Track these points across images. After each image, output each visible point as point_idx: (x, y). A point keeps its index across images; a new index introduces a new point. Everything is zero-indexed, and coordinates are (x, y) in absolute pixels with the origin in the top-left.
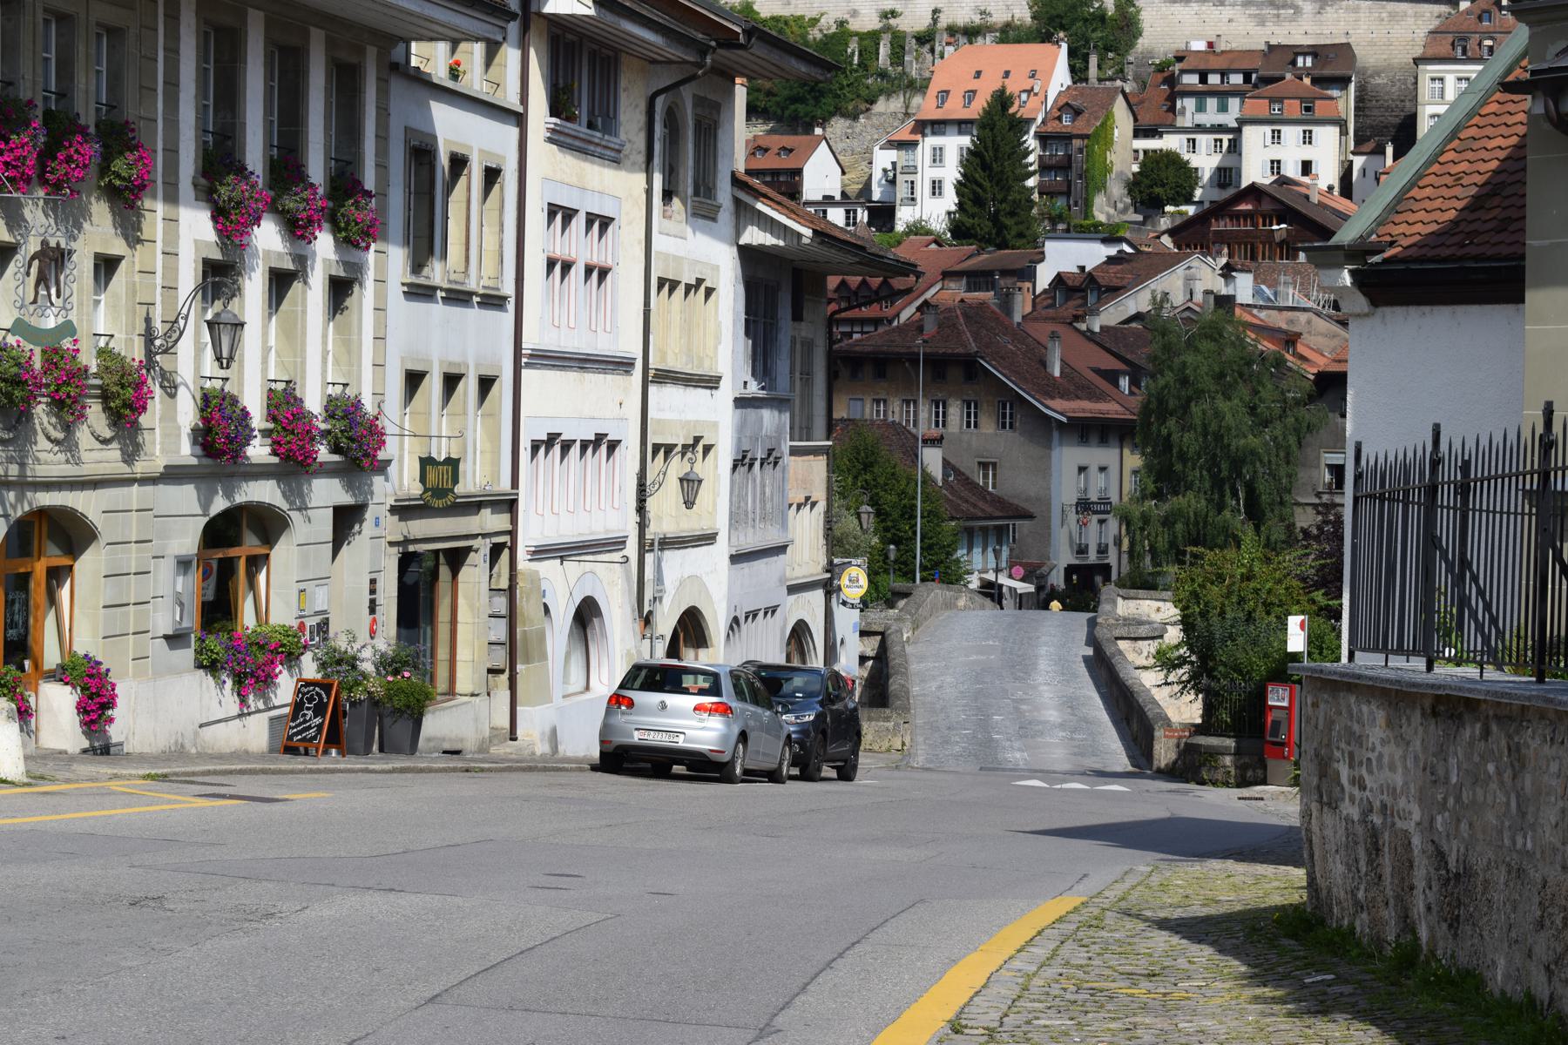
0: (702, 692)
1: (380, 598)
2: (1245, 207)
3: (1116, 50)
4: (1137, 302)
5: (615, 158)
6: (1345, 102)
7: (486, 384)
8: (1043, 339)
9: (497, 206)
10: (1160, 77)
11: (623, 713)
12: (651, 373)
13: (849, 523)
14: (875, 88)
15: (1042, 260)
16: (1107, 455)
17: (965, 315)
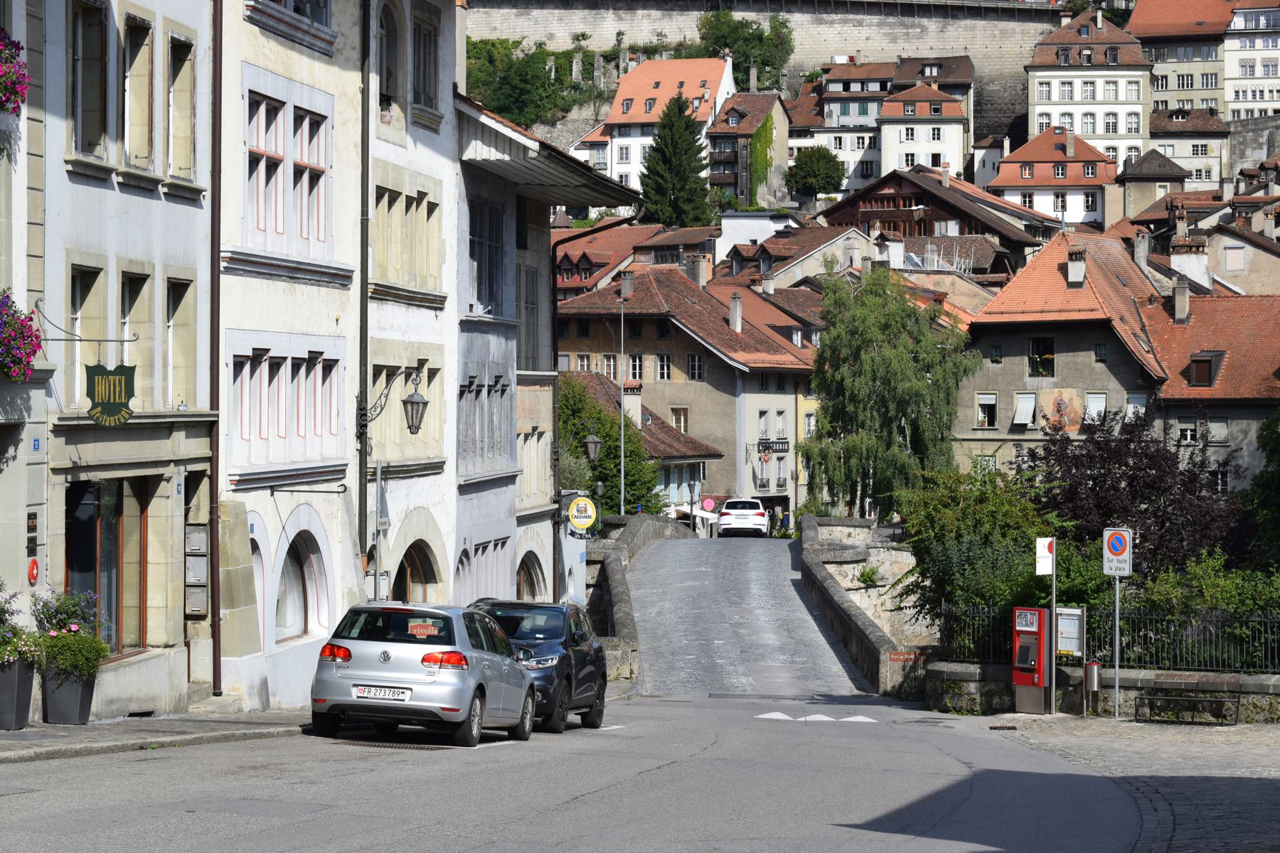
0: (430, 640)
1: (42, 536)
2: (888, 191)
3: (772, 65)
4: (810, 266)
5: (327, 51)
6: (966, 105)
7: (177, 289)
8: (725, 300)
9: (188, 87)
10: (810, 86)
11: (339, 667)
12: (371, 288)
13: (567, 460)
14: (569, 99)
15: (719, 236)
16: (784, 401)
17: (658, 281)
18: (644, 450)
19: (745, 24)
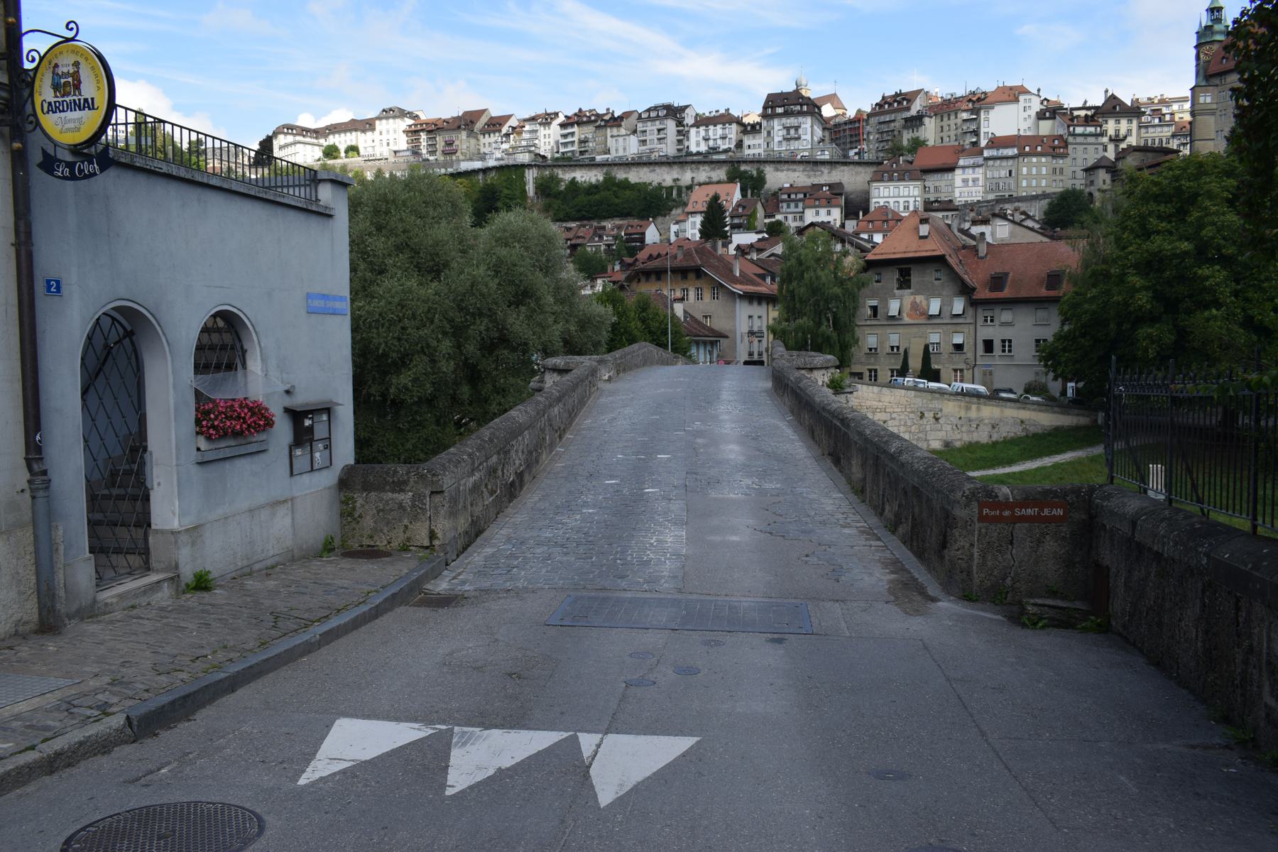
18: (684, 331)
19: (746, 172)
